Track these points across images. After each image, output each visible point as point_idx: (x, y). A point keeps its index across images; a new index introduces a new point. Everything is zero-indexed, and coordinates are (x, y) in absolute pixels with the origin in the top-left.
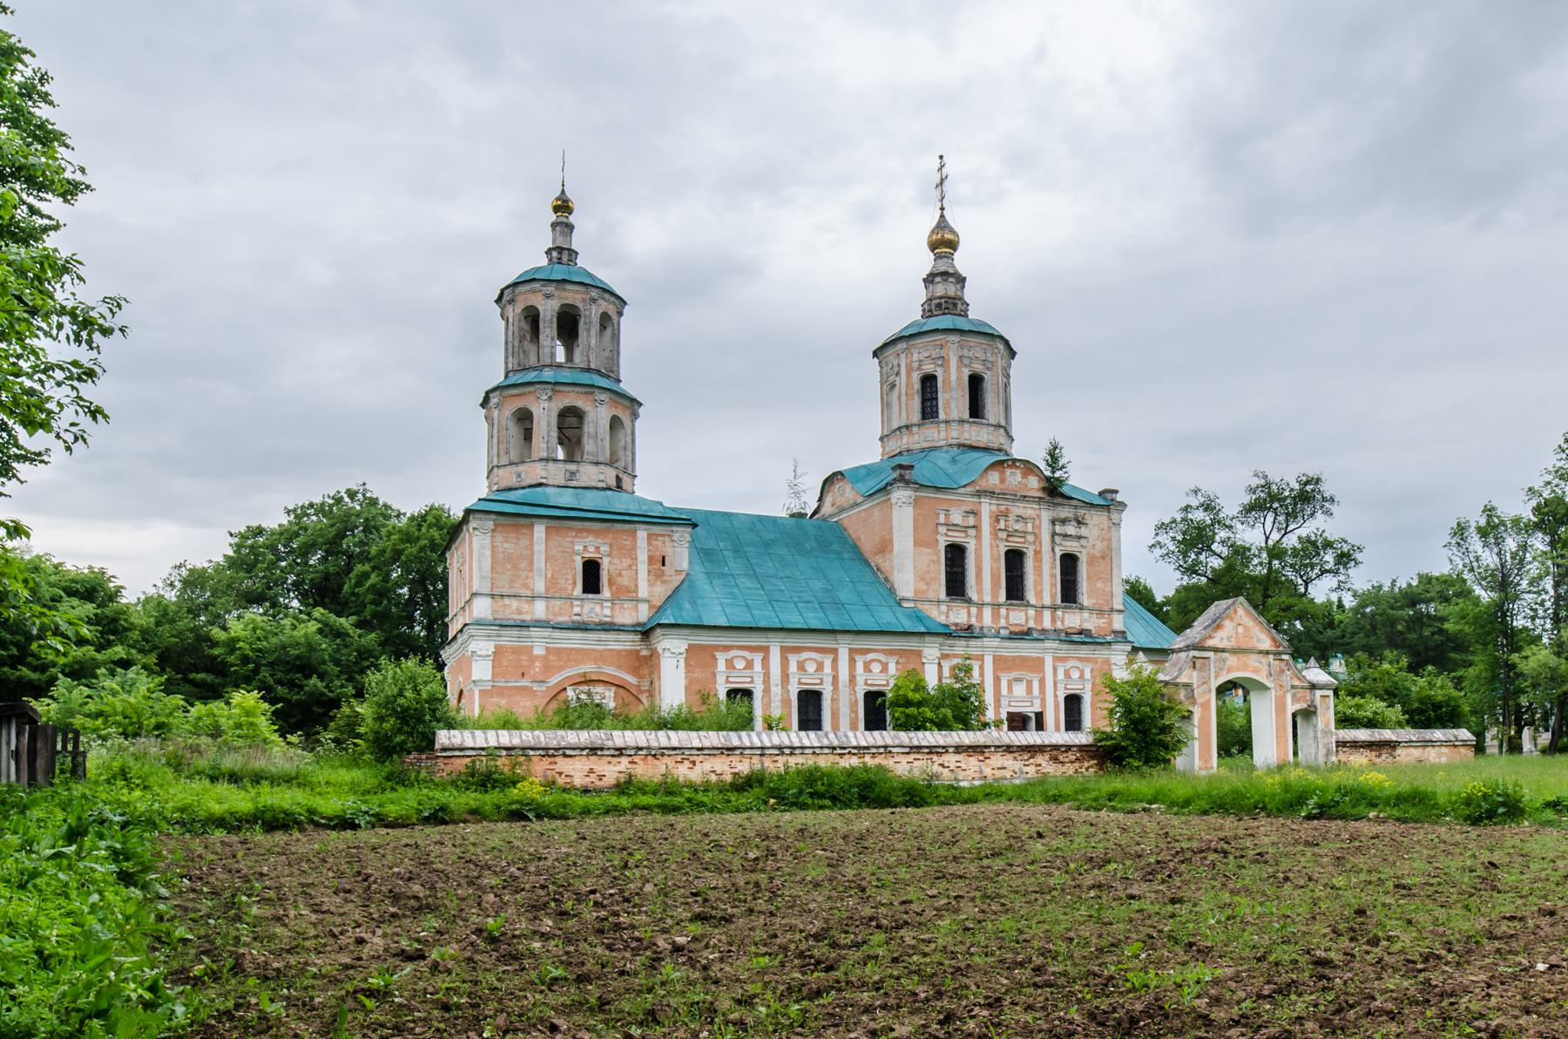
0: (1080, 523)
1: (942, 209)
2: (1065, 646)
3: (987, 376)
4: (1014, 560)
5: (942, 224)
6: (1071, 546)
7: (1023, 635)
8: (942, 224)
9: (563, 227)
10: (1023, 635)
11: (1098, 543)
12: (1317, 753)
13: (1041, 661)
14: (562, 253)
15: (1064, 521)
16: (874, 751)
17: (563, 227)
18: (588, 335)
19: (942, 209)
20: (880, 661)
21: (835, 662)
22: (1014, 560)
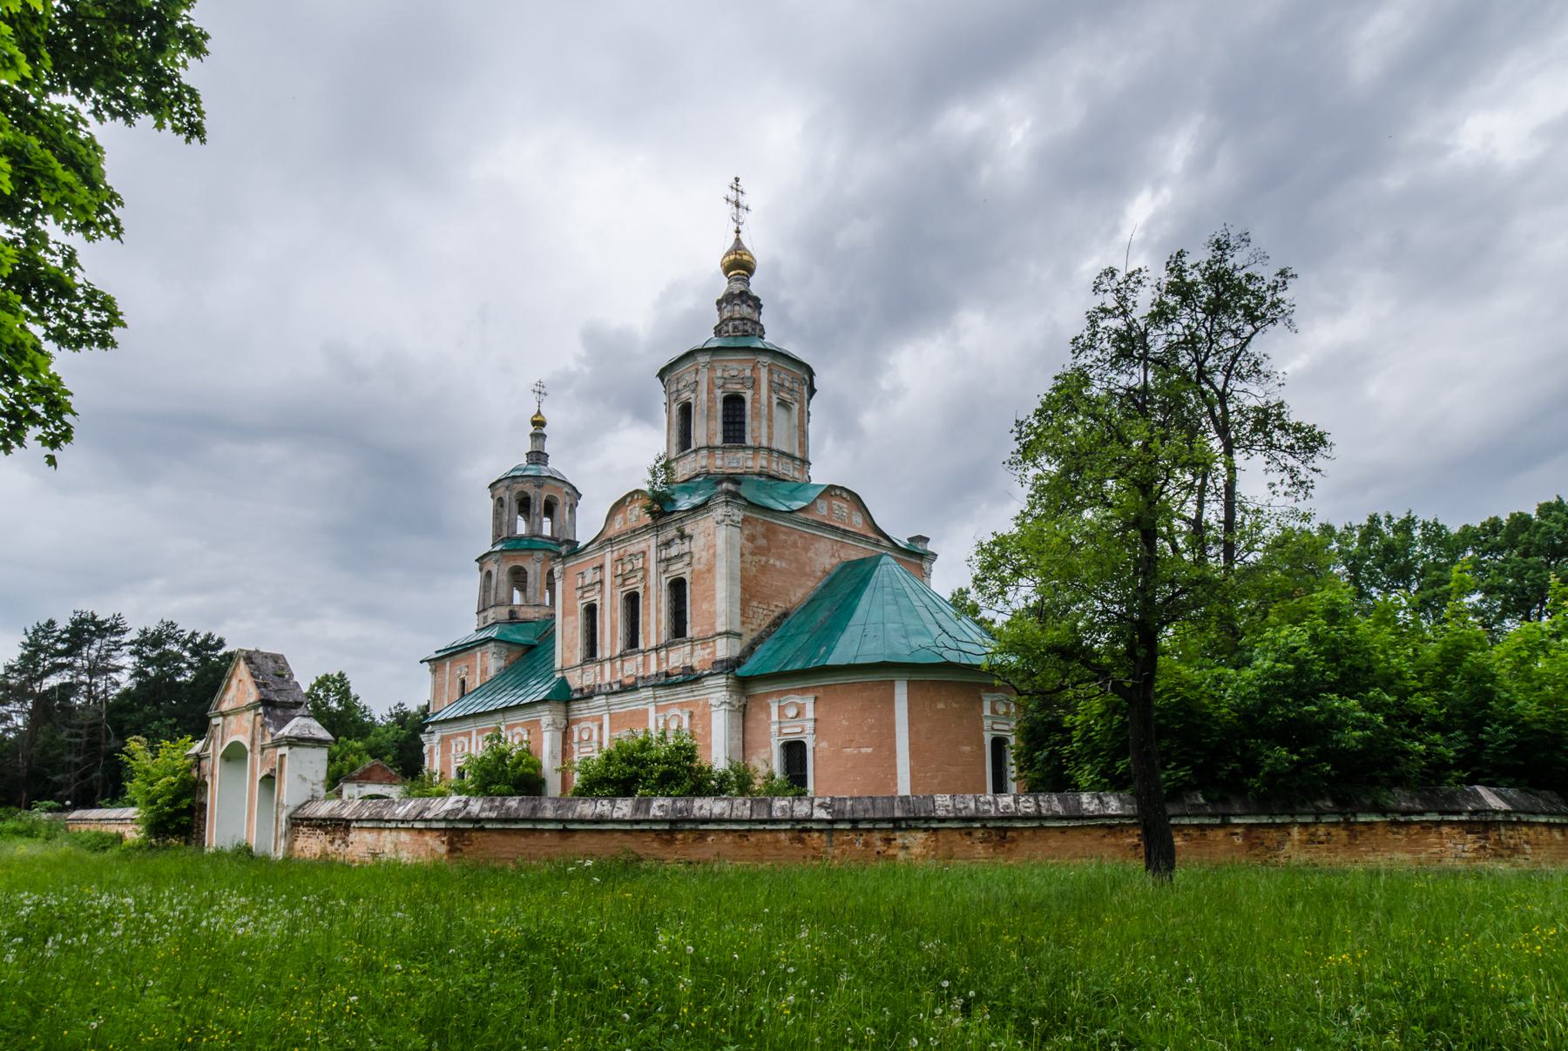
0: (682, 536)
1: (738, 232)
2: (660, 692)
3: (748, 395)
4: (632, 600)
5: (738, 245)
6: (677, 569)
7: (626, 689)
8: (738, 245)
9: (538, 436)
10: (626, 689)
11: (704, 553)
12: (785, 830)
13: (646, 711)
14: (538, 457)
15: (668, 544)
16: (418, 825)
17: (538, 436)
18: (562, 511)
19: (738, 232)
20: (796, 704)
21: (601, 727)
22: (632, 600)
